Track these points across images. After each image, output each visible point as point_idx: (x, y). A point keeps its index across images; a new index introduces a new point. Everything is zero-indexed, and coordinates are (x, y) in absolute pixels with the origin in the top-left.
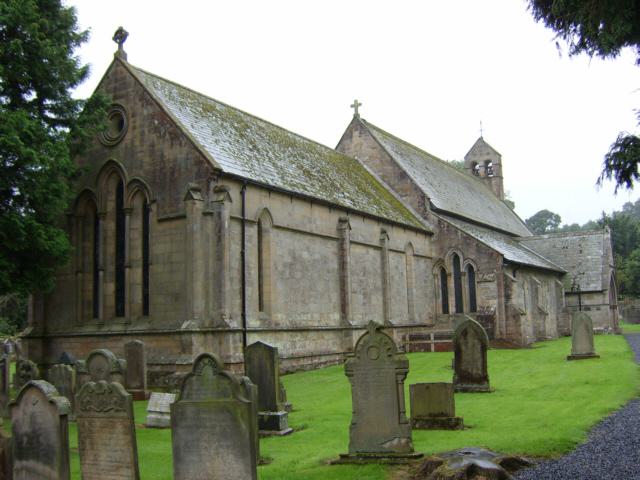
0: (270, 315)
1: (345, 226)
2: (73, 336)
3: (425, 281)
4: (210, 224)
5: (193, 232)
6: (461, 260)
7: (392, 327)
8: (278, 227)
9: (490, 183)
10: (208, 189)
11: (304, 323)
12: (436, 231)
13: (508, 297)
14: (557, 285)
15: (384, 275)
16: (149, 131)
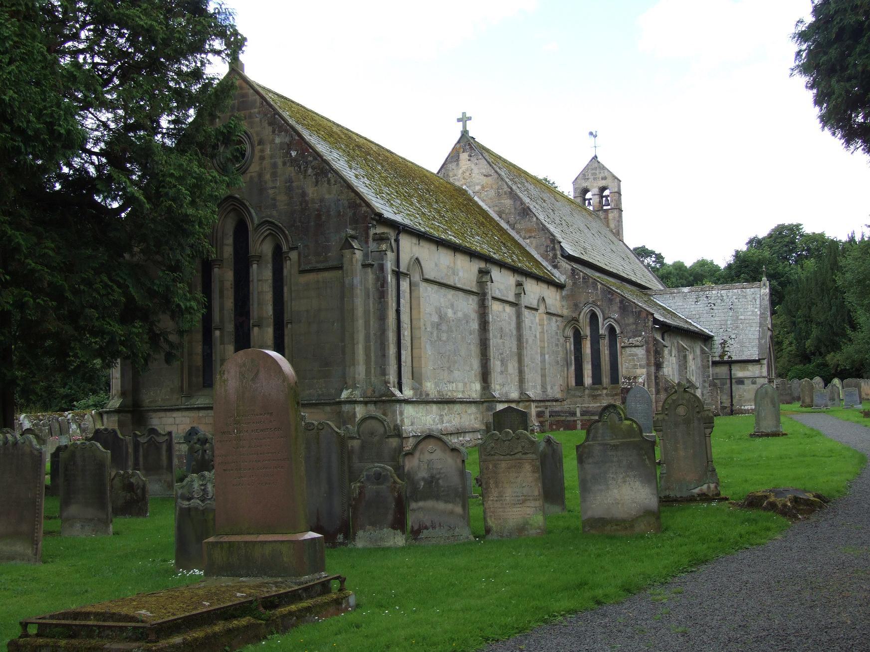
0: (421, 384)
1: (487, 278)
2: (178, 410)
3: (557, 345)
4: (371, 276)
5: (352, 287)
6: (600, 320)
7: (530, 400)
8: (427, 280)
9: (607, 218)
10: (367, 237)
11: (449, 394)
12: (570, 283)
13: (659, 366)
14: (703, 352)
15: (520, 338)
16: (284, 164)
